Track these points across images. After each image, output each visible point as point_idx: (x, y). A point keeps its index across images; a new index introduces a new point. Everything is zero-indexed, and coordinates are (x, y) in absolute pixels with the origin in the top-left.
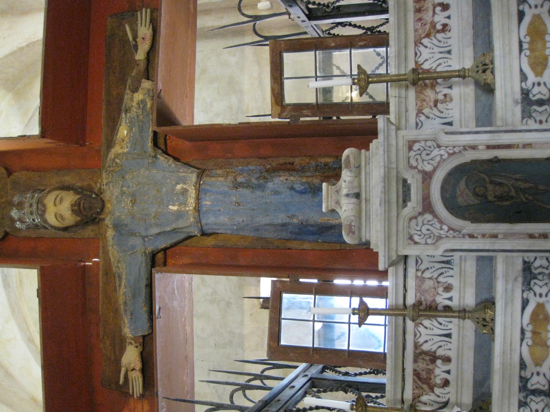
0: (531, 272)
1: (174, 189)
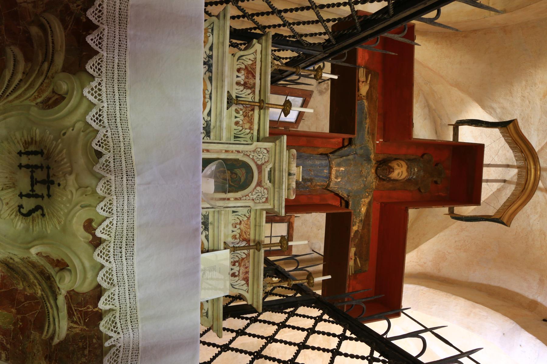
0: (206, 131)
1: (342, 179)
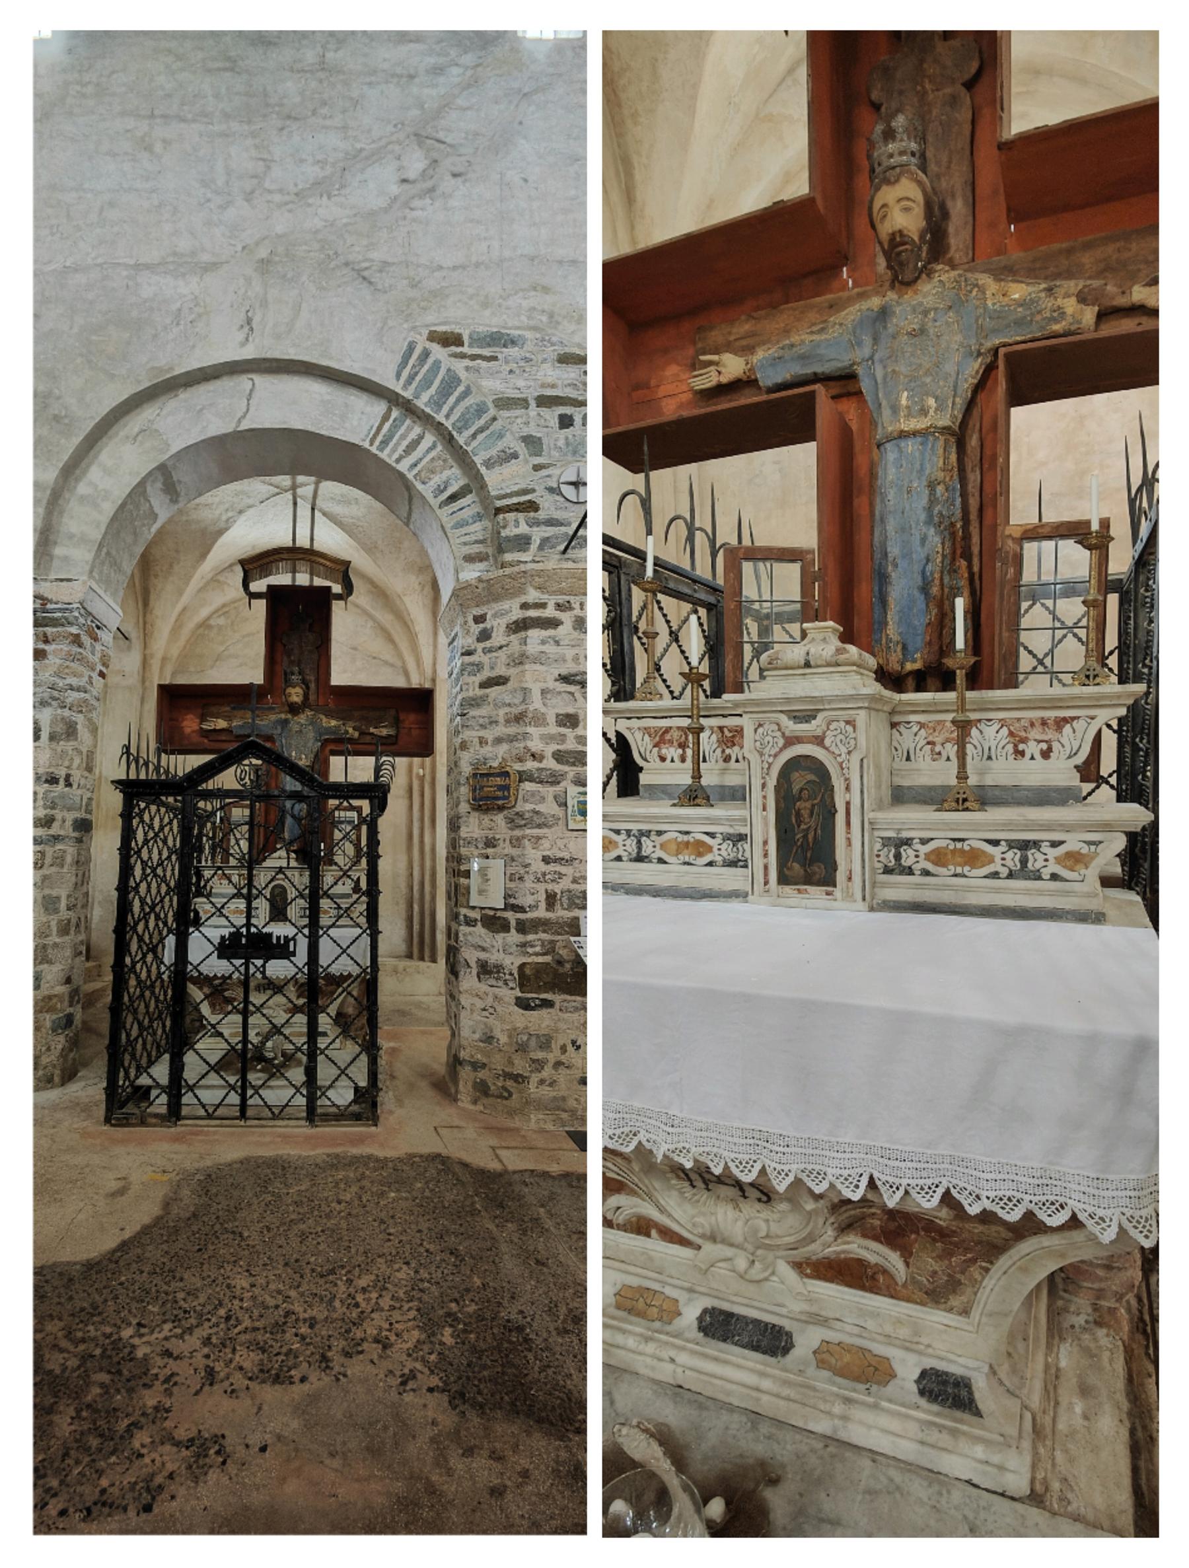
1: (927, 394)
